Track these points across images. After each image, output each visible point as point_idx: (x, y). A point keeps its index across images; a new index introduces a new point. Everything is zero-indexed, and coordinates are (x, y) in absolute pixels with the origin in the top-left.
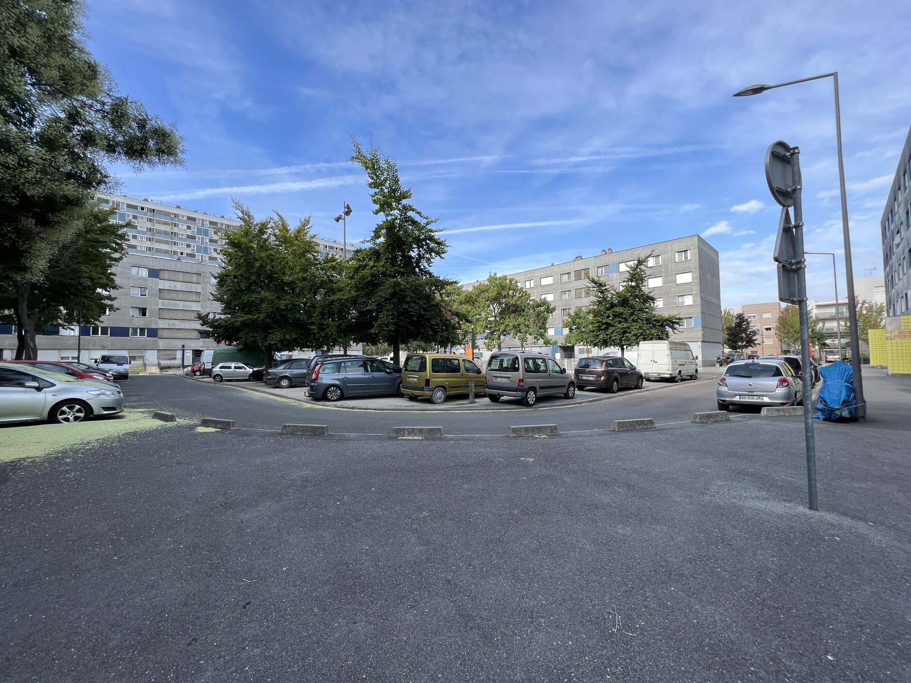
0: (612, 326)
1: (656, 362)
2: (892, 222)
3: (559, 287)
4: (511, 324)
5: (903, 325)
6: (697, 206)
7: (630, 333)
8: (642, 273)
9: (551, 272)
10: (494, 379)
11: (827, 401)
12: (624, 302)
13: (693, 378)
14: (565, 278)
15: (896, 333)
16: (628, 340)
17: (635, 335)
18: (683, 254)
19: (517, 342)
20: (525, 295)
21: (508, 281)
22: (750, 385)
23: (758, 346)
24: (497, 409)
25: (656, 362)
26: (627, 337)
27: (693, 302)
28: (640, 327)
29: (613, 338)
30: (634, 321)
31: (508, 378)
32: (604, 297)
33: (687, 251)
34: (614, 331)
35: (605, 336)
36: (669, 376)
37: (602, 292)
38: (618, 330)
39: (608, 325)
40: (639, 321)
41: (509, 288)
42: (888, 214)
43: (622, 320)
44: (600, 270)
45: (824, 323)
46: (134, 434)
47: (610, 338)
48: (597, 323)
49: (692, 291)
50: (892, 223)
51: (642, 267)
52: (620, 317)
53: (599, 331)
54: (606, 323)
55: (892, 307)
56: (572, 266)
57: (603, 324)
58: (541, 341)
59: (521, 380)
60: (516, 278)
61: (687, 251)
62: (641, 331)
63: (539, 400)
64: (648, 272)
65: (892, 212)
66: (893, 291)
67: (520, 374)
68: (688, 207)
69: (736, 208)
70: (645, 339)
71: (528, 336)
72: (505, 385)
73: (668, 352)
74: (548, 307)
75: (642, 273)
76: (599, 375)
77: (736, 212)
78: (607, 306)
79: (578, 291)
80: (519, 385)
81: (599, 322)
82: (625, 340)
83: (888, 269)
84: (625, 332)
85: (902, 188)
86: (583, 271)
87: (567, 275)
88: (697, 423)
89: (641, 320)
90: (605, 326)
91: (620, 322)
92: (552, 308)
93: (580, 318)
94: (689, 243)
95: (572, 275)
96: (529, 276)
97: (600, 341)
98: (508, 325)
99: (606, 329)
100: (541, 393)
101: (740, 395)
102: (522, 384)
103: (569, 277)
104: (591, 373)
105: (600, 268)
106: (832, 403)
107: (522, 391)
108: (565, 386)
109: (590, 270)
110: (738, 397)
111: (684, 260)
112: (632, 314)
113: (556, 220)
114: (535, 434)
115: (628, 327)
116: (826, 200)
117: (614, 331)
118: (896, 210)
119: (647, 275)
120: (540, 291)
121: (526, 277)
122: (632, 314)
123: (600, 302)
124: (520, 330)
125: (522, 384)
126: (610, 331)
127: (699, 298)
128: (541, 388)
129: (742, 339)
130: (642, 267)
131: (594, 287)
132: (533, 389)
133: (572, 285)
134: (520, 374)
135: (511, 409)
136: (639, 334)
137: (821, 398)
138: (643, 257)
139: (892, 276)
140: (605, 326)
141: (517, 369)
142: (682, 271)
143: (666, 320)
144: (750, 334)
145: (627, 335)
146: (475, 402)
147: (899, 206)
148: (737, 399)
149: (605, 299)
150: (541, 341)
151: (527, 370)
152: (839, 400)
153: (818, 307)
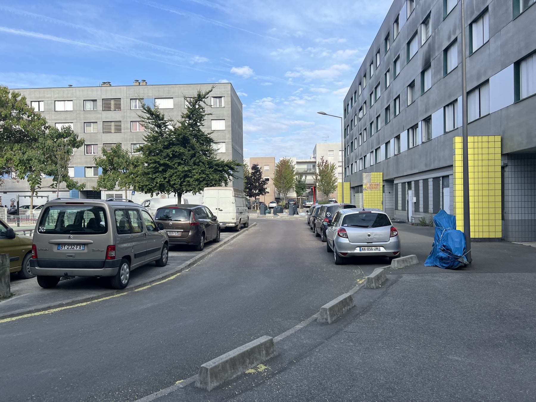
0: (171, 168)
1: (221, 210)
2: (355, 101)
3: (82, 116)
4: (16, 159)
5: (372, 179)
6: (204, 59)
7: (191, 177)
8: (201, 110)
9: (69, 95)
10: (55, 249)
11: (453, 251)
12: (184, 141)
13: (246, 225)
14: (89, 106)
15: (369, 185)
16: (189, 185)
17: (197, 180)
18: (218, 100)
19: (25, 184)
20: (37, 118)
21: (10, 96)
22: (369, 235)
23: (267, 194)
24: (67, 304)
25: (221, 210)
26: (188, 182)
27: (226, 150)
28: (202, 171)
29: (172, 183)
30: (195, 164)
31: (84, 244)
32: (161, 133)
33: (221, 97)
34: (173, 174)
35: (162, 180)
36: (234, 225)
37: (159, 126)
38: (178, 174)
39: (167, 167)
40: (200, 163)
41: (13, 106)
42: (353, 95)
43: (182, 162)
44: (133, 103)
45: (306, 176)
46: (242, 67)
47: (169, 182)
48: (153, 163)
49: (225, 139)
50: (355, 103)
51: (201, 103)
52: (179, 158)
53: (155, 173)
54: (164, 165)
55: (350, 166)
56: (99, 93)
57: (161, 165)
58: (64, 184)
59: (111, 248)
60: (23, 93)
61: (221, 97)
62: (204, 176)
63: (134, 273)
64: (207, 110)
65: (355, 93)
66: (352, 154)
67: (110, 237)
68: (197, 58)
69: (234, 70)
70: (208, 185)
71: (43, 175)
72: (78, 258)
73: (232, 199)
74: (75, 139)
75: (201, 110)
76: (185, 228)
77: (234, 74)
78: (166, 144)
79: (106, 124)
80: (107, 257)
81: (155, 162)
82: (186, 185)
83: (348, 137)
84: (186, 176)
85: (368, 75)
86: (112, 101)
87: (92, 102)
88: (373, 289)
89: (203, 163)
90: (162, 168)
91: (179, 164)
92: (80, 141)
93: (119, 157)
94: (223, 90)
95: (100, 103)
96: (38, 95)
97: (156, 185)
98: (11, 159)
99: (164, 171)
100: (135, 264)
101: (360, 247)
102: (113, 254)
103: (95, 106)
104: (175, 227)
105: (134, 101)
106: (455, 252)
107: (112, 265)
108: (159, 249)
109: (122, 100)
110: (358, 248)
111: (218, 107)
112: (193, 155)
113: (58, 36)
114: (247, 368)
115: (189, 171)
116: (290, 79)
117: (173, 174)
118: (360, 93)
119: (206, 113)
120: (53, 117)
121: (33, 95)
122: (193, 155)
123: (155, 139)
124: (30, 167)
125: (113, 254)
126: (167, 175)
127: (230, 146)
128: (136, 256)
129: (255, 188)
130: (201, 103)
131: (148, 119)
132: (127, 259)
133: (99, 116)
134: (110, 237)
135: (93, 299)
136: (201, 179)
137: (444, 246)
138: (203, 92)
139: (352, 143)
140: (162, 168)
141: (105, 230)
142: (217, 117)
143: (227, 165)
144: (262, 183)
145: (188, 179)
146: (12, 295)
147: (363, 89)
148: (357, 250)
149: (161, 134)
150: (64, 184)
151: (120, 230)
152: (461, 247)
153: (298, 163)
